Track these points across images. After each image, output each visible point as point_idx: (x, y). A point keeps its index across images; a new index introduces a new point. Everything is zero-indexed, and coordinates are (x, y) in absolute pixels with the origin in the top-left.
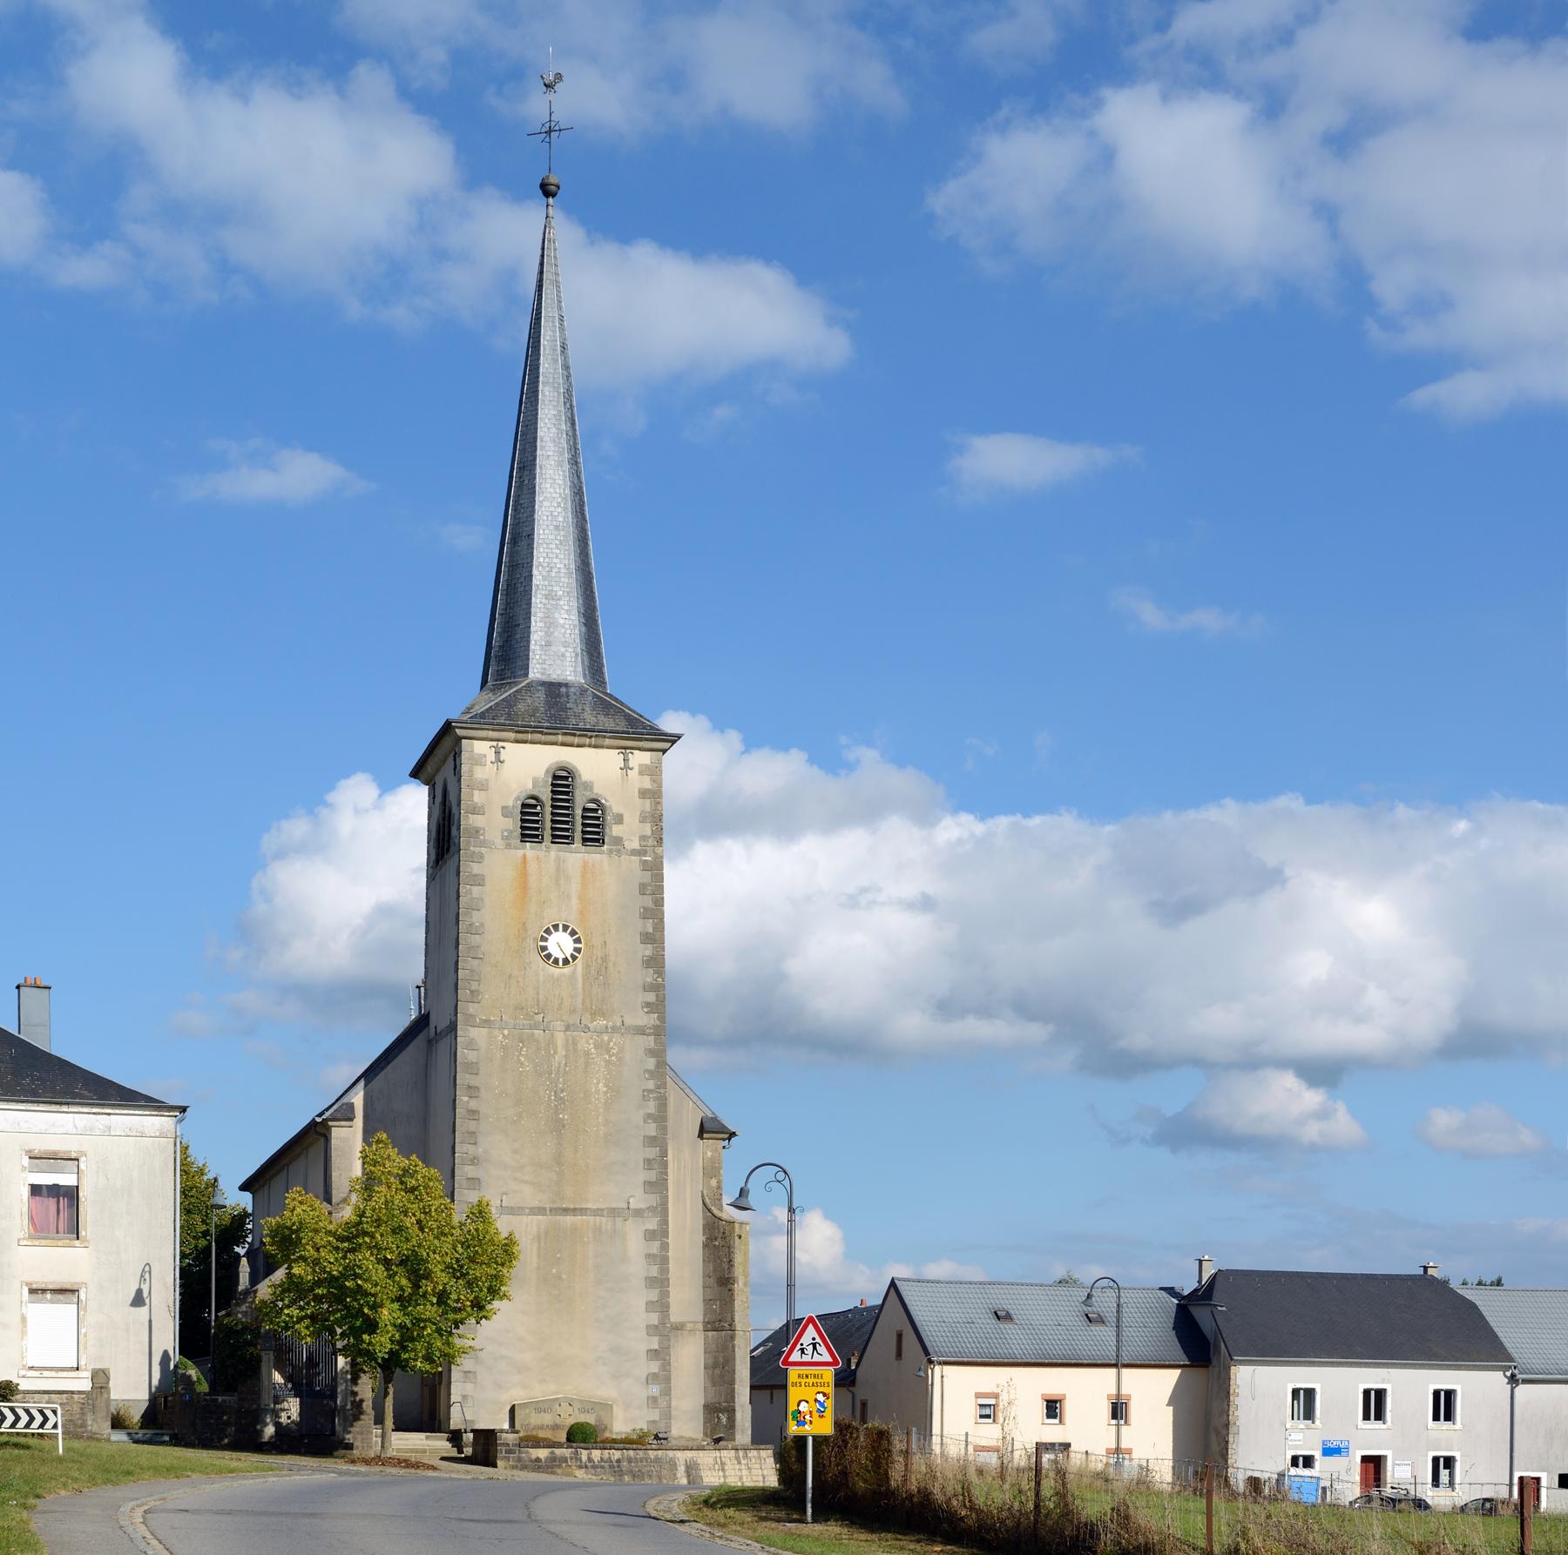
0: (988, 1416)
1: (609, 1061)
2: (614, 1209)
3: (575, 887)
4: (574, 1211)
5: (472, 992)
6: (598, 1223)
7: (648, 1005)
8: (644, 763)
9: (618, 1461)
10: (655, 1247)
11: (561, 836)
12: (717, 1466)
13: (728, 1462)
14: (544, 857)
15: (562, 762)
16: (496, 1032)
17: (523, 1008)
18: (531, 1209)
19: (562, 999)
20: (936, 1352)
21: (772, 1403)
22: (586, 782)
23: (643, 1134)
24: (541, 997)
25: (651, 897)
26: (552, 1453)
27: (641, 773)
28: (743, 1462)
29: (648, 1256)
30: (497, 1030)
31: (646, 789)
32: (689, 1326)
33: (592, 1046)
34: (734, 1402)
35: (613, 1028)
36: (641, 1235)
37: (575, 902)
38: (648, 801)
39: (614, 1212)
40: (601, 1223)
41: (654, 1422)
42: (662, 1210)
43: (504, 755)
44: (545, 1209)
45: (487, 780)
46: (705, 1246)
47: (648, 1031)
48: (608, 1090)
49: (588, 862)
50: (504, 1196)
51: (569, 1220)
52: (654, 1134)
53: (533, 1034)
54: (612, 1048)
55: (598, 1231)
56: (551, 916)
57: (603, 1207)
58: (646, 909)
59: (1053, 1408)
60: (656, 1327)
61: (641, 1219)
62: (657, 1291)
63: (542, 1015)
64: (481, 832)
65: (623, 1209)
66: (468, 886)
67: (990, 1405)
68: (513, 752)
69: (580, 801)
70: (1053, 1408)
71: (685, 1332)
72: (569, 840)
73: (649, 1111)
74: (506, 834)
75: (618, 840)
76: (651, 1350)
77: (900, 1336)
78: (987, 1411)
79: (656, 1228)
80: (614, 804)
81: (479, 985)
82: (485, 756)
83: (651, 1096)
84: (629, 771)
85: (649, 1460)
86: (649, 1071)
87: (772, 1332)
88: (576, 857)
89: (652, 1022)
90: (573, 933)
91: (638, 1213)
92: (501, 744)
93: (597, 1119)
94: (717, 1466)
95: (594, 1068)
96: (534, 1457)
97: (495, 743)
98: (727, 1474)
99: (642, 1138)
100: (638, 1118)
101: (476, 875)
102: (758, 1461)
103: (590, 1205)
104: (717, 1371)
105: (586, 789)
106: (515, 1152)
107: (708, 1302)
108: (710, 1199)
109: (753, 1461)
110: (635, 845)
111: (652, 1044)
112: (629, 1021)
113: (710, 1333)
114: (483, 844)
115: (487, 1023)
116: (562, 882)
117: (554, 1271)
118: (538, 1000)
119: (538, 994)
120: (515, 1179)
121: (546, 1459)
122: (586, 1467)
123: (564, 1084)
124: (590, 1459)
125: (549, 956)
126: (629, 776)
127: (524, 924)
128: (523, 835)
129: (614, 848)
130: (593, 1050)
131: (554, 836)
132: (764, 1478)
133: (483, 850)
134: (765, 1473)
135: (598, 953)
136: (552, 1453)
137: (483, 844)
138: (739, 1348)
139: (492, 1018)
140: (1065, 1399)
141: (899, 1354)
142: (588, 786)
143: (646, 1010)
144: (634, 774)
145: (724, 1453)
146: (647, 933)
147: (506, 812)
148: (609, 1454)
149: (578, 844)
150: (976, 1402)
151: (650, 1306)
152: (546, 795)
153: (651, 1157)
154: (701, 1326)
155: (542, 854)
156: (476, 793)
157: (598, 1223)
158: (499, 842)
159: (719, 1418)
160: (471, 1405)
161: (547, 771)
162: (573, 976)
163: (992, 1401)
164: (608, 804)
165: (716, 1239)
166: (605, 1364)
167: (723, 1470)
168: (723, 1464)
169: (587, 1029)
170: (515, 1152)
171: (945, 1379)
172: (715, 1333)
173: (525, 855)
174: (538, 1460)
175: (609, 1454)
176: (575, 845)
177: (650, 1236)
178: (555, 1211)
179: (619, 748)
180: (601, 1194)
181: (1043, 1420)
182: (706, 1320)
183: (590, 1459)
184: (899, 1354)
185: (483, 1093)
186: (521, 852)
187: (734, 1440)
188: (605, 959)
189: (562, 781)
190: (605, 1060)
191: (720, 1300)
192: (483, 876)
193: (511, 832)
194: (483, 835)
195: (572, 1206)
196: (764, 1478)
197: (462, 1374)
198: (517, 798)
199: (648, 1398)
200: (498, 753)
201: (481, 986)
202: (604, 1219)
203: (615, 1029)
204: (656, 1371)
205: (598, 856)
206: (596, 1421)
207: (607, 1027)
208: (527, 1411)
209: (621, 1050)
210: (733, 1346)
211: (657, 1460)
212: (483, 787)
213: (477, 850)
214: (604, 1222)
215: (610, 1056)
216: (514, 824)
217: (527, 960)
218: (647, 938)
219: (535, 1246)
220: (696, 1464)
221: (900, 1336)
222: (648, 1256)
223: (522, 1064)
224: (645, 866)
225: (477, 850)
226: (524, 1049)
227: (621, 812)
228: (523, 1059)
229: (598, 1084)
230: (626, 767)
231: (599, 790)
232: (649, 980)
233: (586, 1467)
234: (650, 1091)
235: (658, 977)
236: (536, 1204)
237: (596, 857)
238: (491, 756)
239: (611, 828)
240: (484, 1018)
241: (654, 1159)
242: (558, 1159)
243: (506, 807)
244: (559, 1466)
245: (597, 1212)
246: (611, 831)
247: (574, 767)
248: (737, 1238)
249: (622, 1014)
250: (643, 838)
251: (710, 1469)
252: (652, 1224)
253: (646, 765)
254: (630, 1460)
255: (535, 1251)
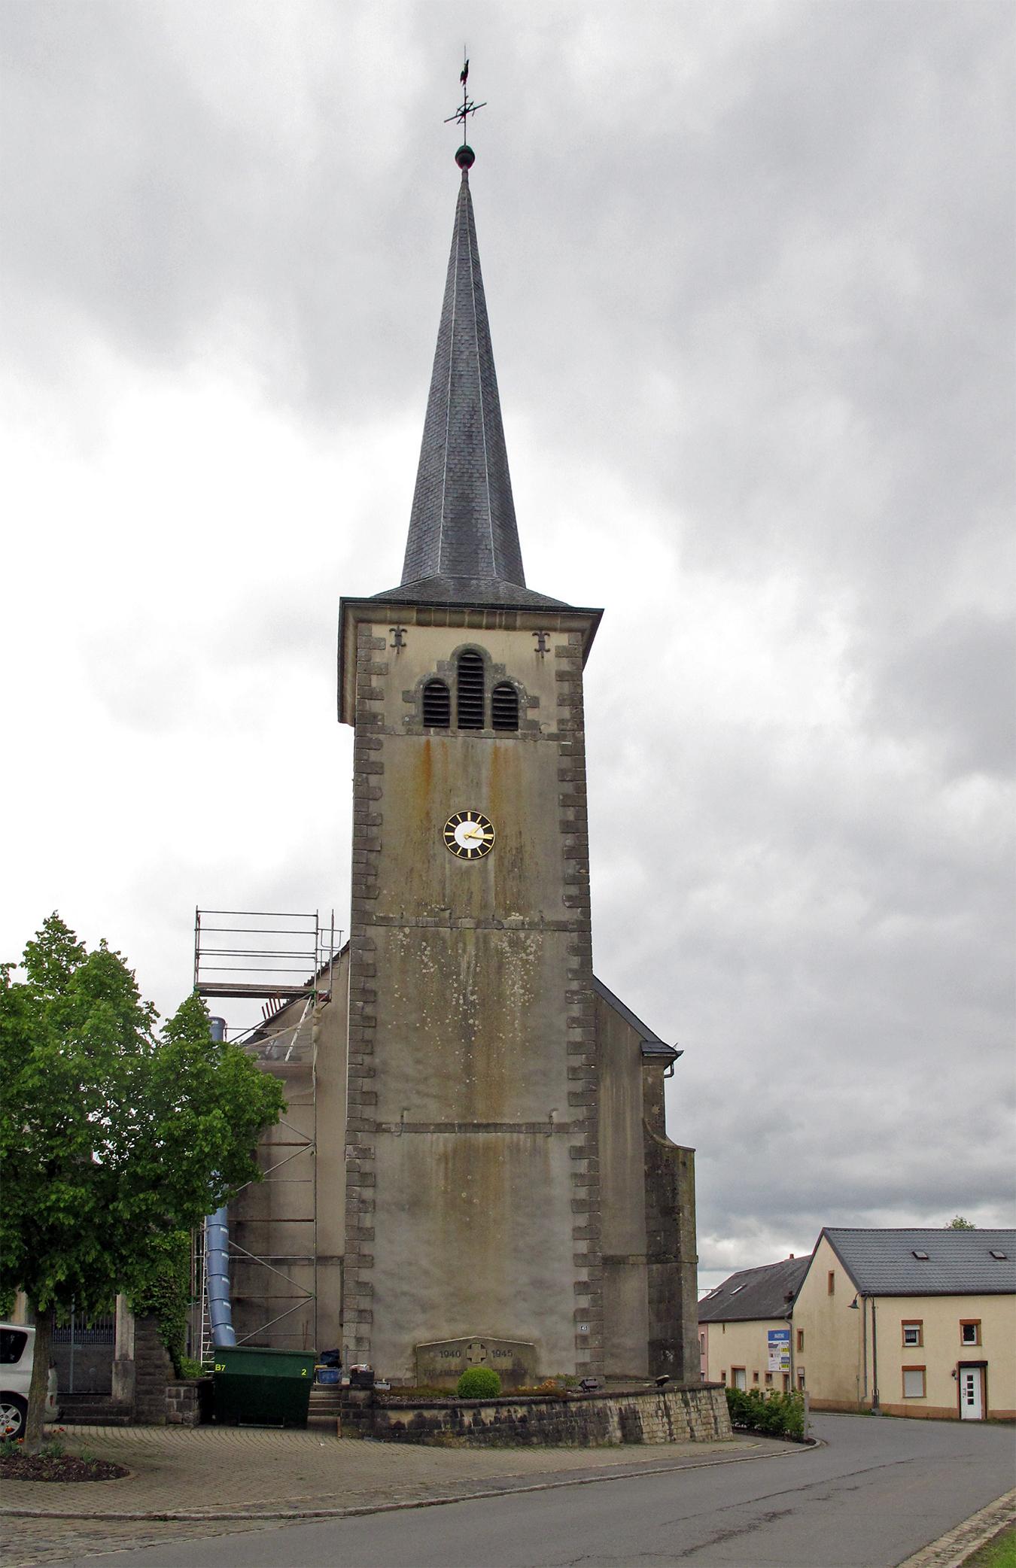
0: (914, 1341)
1: (527, 960)
2: (534, 1124)
3: (485, 773)
4: (486, 1127)
5: (368, 887)
6: (515, 1139)
7: (570, 898)
8: (561, 644)
9: (523, 1420)
10: (583, 1166)
11: (471, 720)
12: (660, 1412)
13: (673, 1405)
14: (448, 744)
15: (469, 644)
16: (395, 931)
17: (426, 904)
18: (438, 1125)
19: (472, 893)
20: (151, 1537)
21: (724, 1332)
22: (496, 665)
23: (566, 1039)
24: (448, 892)
25: (571, 784)
26: (420, 1416)
27: (558, 655)
28: (691, 1404)
29: (575, 1176)
30: (397, 928)
31: (564, 672)
32: (631, 1260)
33: (506, 944)
34: (681, 1339)
35: (530, 924)
36: (566, 1154)
37: (485, 790)
38: (566, 684)
39: (533, 1128)
40: (519, 1140)
41: (584, 1364)
42: (591, 1124)
43: (405, 638)
44: (453, 1125)
45: (387, 665)
46: (647, 1175)
47: (571, 926)
48: (525, 992)
49: (500, 748)
50: (405, 1113)
51: (482, 1137)
52: (578, 1039)
53: (438, 933)
54: (530, 946)
55: (515, 1149)
56: (459, 803)
57: (521, 1122)
58: (566, 796)
59: (970, 1330)
60: (585, 1255)
61: (566, 1135)
62: (587, 1215)
63: (449, 911)
64: (380, 717)
65: (544, 1124)
66: (364, 775)
67: (915, 1331)
68: (414, 635)
69: (490, 682)
70: (970, 1330)
71: (627, 1266)
72: (478, 724)
73: (574, 1015)
74: (407, 719)
75: (534, 725)
76: (579, 1283)
77: (832, 1275)
78: (913, 1337)
79: (583, 1144)
80: (526, 685)
81: (376, 880)
82: (384, 640)
83: (576, 998)
84: (545, 653)
85: (569, 1414)
86: (571, 970)
87: (726, 1276)
88: (489, 742)
89: (575, 917)
90: (483, 822)
91: (562, 1129)
92: (402, 627)
93: (513, 1024)
94: (660, 1412)
95: (509, 969)
96: (393, 1421)
97: (395, 627)
98: (672, 1419)
99: (565, 1045)
100: (561, 1021)
101: (373, 763)
102: (708, 1402)
103: (506, 1121)
104: (663, 1306)
105: (496, 671)
106: (418, 1062)
107: (651, 1234)
108: (651, 1126)
109: (703, 1401)
110: (553, 728)
111: (576, 940)
112: (550, 916)
113: (654, 1267)
114: (382, 730)
115: (385, 921)
116: (470, 769)
117: (464, 1195)
118: (444, 896)
119: (444, 888)
120: (418, 1093)
121: (411, 1423)
122: (471, 1432)
123: (474, 987)
124: (477, 1421)
125: (456, 847)
126: (545, 659)
127: (428, 813)
128: (426, 720)
129: (530, 732)
130: (507, 949)
131: (460, 720)
132: (716, 1419)
133: (381, 737)
134: (717, 1414)
135: (513, 843)
136: (420, 1416)
137: (382, 730)
138: (686, 1281)
139: (391, 916)
140: (980, 1323)
141: (831, 1290)
142: (500, 669)
143: (567, 904)
144: (549, 657)
145: (670, 1397)
146: (568, 821)
147: (407, 697)
148: (509, 1411)
149: (488, 730)
150: (903, 1328)
151: (578, 1233)
152: (451, 679)
153: (577, 1064)
154: (643, 1259)
155: (447, 740)
156: (374, 678)
157: (515, 1139)
158: (401, 729)
159: (665, 1355)
160: (367, 1348)
161: (453, 654)
162: (484, 870)
163: (917, 1328)
164: (521, 687)
165: (658, 1168)
166: (524, 1300)
167: (668, 1416)
168: (667, 1408)
169: (501, 927)
170: (418, 1062)
171: (876, 1310)
172: (659, 1266)
173: (428, 742)
174: (399, 1426)
175: (509, 1411)
176: (485, 729)
177: (577, 1153)
178: (465, 1127)
179: (535, 629)
180: (517, 1109)
181: (962, 1342)
182: (650, 1252)
183: (477, 1421)
184: (831, 1290)
185: (381, 997)
186: (424, 738)
187: (682, 1379)
188: (520, 850)
189: (471, 663)
190: (521, 959)
191: (665, 1231)
192: (381, 763)
193: (412, 717)
194: (382, 719)
195: (484, 1121)
196: (716, 1419)
197: (357, 1313)
198: (420, 682)
199: (576, 1337)
200: (398, 636)
201: (379, 880)
202: (522, 1136)
203: (532, 926)
204: (586, 1306)
205: (510, 743)
206: (514, 1365)
207: (523, 923)
208: (432, 1354)
209: (540, 947)
210: (680, 1279)
211: (580, 1412)
212: (383, 671)
213: (374, 736)
214: (523, 1139)
215: (527, 955)
216: (415, 709)
217: (431, 852)
218: (568, 826)
219: (443, 1166)
220: (635, 1412)
221: (832, 1275)
222: (575, 1176)
223: (426, 965)
224: (565, 752)
225: (374, 736)
226: (429, 948)
227: (536, 695)
228: (426, 960)
229: (514, 985)
230: (541, 649)
231: (511, 673)
232: (570, 871)
233: (471, 1432)
234: (573, 993)
235: (581, 869)
236: (443, 1119)
237: (507, 743)
238: (391, 639)
239: (525, 711)
240: (381, 915)
241: (580, 1067)
242: (468, 1069)
243: (408, 692)
244: (430, 1434)
245: (514, 1128)
246: (526, 715)
247: (483, 649)
248: (680, 1165)
249: (541, 908)
250: (561, 722)
251: (652, 1417)
252: (579, 1140)
253: (563, 646)
254: (541, 1417)
255: (441, 1174)
